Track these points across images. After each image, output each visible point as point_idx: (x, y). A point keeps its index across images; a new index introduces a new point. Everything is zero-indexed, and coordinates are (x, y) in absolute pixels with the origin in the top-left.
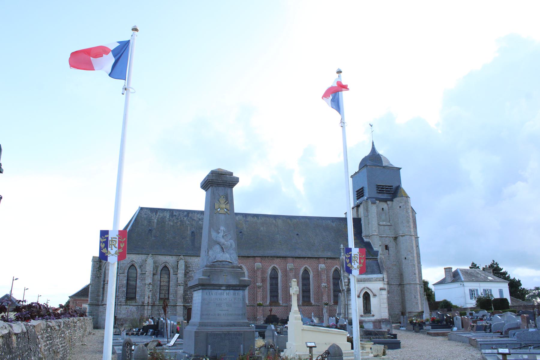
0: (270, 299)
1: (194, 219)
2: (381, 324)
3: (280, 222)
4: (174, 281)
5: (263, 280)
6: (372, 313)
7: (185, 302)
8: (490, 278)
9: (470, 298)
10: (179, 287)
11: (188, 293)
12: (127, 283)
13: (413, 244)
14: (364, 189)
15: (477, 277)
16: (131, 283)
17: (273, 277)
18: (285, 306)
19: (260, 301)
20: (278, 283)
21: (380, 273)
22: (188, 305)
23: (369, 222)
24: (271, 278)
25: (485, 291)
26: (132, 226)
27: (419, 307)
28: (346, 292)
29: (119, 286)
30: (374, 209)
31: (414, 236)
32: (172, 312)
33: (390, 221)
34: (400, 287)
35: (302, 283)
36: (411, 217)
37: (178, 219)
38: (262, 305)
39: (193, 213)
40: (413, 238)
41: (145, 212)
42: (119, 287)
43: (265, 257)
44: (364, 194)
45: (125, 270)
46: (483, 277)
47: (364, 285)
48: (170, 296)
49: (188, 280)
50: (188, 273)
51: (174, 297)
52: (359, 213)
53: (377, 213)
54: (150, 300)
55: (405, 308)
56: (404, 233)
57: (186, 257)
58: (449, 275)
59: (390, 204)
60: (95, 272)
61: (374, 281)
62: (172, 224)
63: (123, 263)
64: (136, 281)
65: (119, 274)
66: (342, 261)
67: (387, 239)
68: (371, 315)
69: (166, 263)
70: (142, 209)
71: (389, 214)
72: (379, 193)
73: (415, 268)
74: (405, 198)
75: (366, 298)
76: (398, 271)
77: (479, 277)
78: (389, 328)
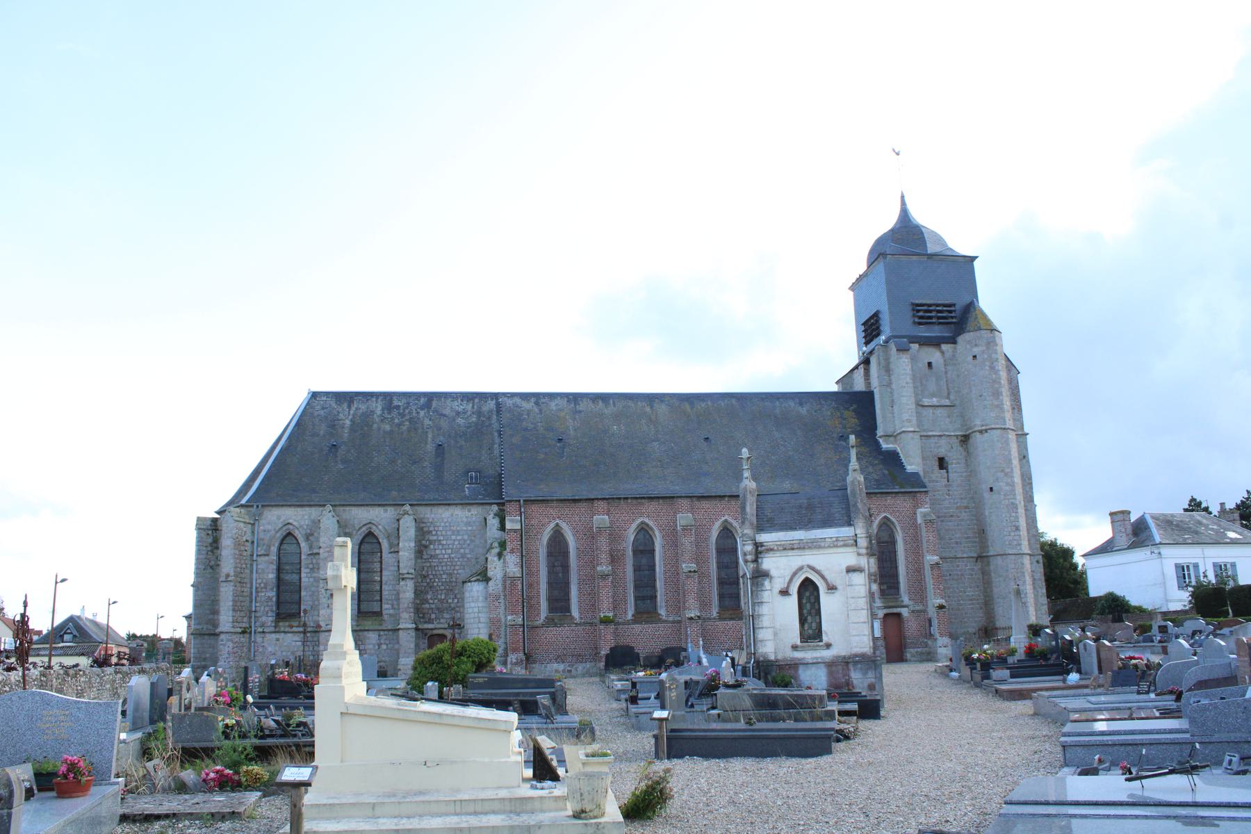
0: (636, 605)
1: (444, 412)
2: (849, 670)
3: (662, 409)
4: (393, 568)
5: (615, 559)
6: (825, 638)
7: (421, 620)
8: (1232, 535)
9: (1179, 587)
10: (402, 583)
11: (429, 597)
12: (279, 578)
13: (1010, 451)
14: (880, 316)
15: (1197, 533)
16: (287, 578)
17: (641, 548)
18: (673, 622)
20: (654, 565)
22: (430, 626)
23: (893, 401)
24: (636, 552)
25: (1219, 568)
26: (289, 438)
27: (1030, 613)
28: (749, 580)
29: (258, 586)
30: (903, 365)
31: (1013, 430)
32: (389, 646)
33: (949, 394)
34: (979, 563)
35: (718, 563)
36: (1004, 381)
37: (403, 415)
38: (613, 622)
39: (443, 399)
40: (1012, 436)
41: (322, 403)
42: (257, 588)
43: (620, 499)
44: (881, 328)
45: (270, 547)
46: (1212, 533)
48: (385, 606)
49: (428, 564)
50: (426, 547)
51: (393, 608)
53: (914, 376)
55: (994, 617)
56: (986, 425)
57: (420, 509)
58: (1123, 530)
59: (948, 351)
60: (203, 554)
61: (829, 547)
62: (388, 428)
63: (265, 531)
64: (300, 573)
65: (255, 558)
66: (744, 495)
67: (943, 441)
68: (821, 644)
69: (370, 525)
70: (315, 395)
71: (946, 377)
72: (920, 324)
73: (1017, 512)
74: (985, 334)
75: (809, 593)
76: (975, 522)
77: (1202, 531)
78: (873, 680)
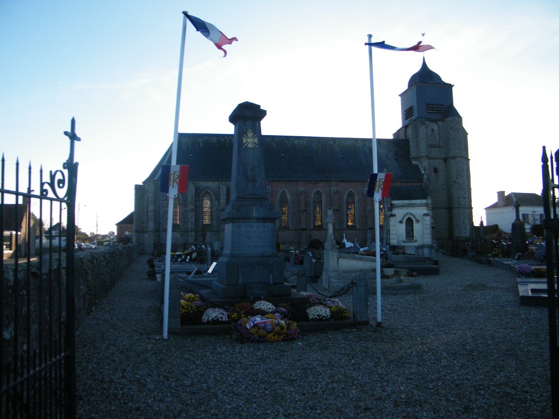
6: (415, 239)
19: (303, 226)
47: (407, 210)
52: (408, 134)
54: (194, 226)
61: (418, 206)
69: (207, 189)
75: (409, 222)
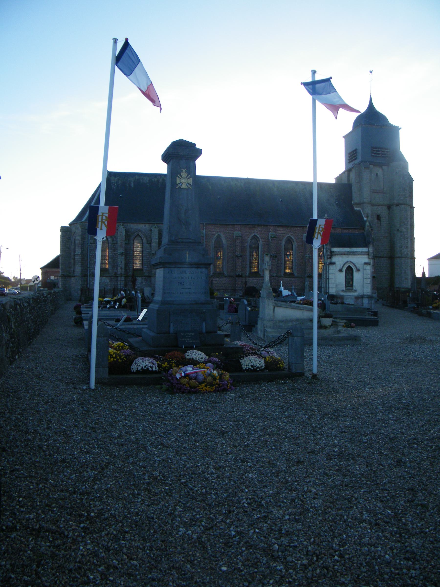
6: (354, 288)
19: (238, 272)
21: (366, 246)
75: (349, 271)
